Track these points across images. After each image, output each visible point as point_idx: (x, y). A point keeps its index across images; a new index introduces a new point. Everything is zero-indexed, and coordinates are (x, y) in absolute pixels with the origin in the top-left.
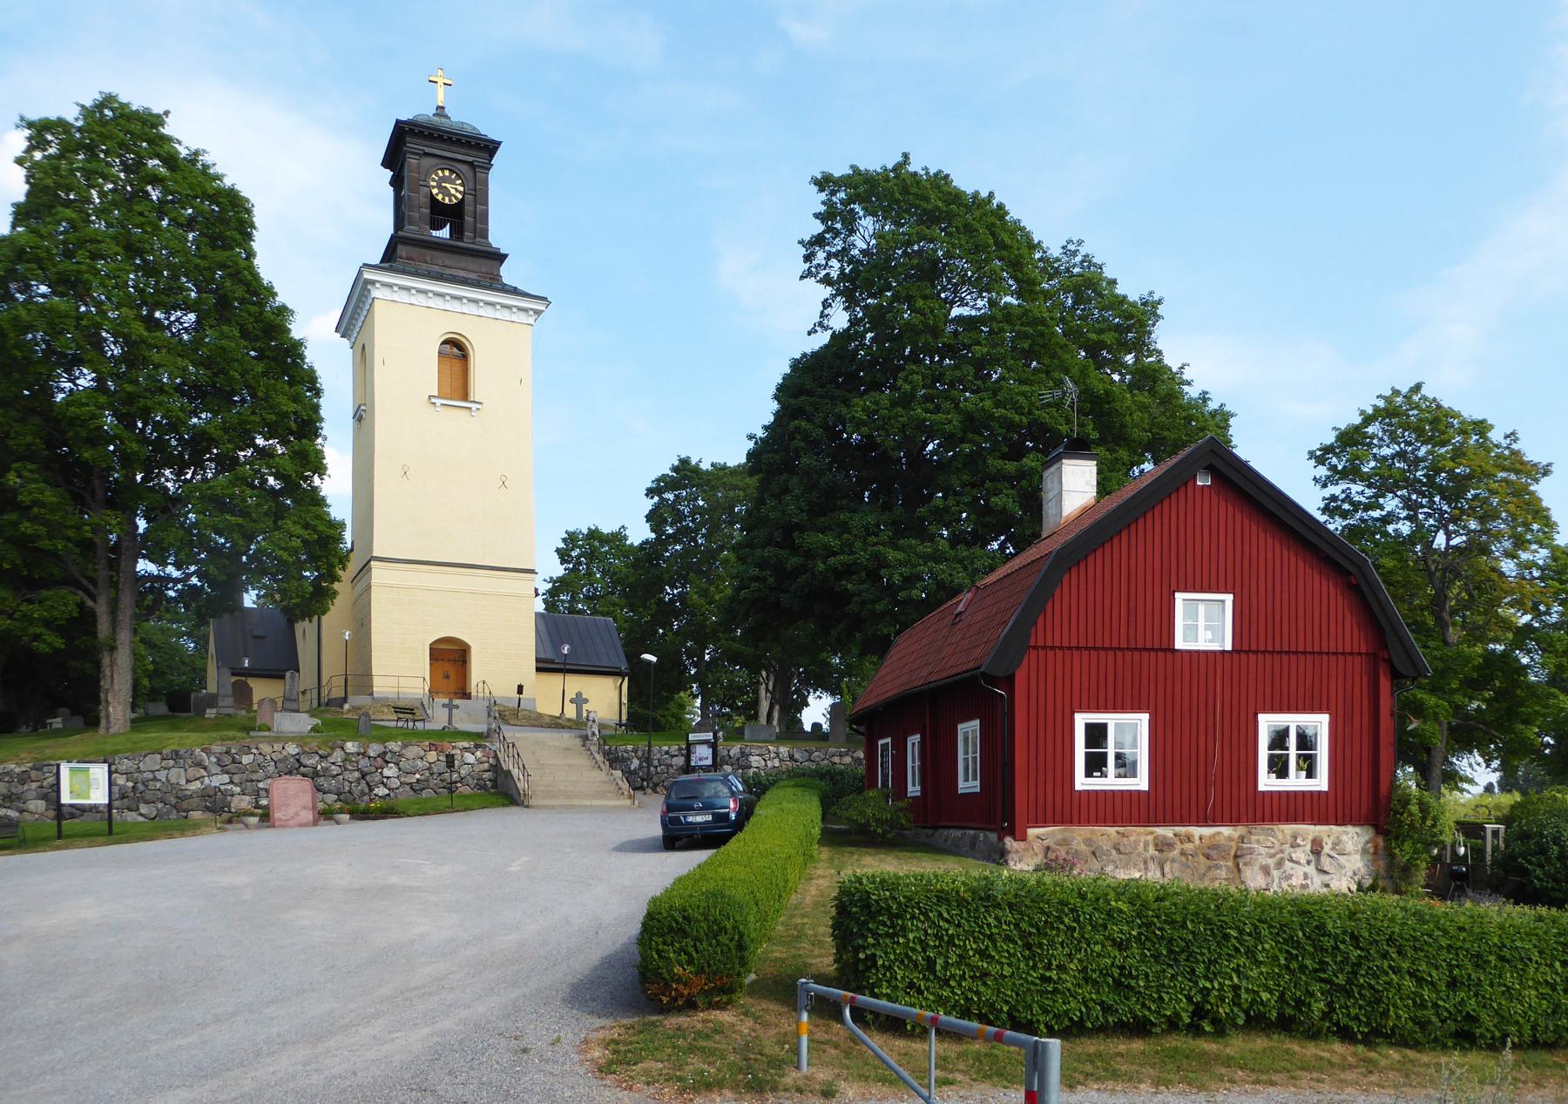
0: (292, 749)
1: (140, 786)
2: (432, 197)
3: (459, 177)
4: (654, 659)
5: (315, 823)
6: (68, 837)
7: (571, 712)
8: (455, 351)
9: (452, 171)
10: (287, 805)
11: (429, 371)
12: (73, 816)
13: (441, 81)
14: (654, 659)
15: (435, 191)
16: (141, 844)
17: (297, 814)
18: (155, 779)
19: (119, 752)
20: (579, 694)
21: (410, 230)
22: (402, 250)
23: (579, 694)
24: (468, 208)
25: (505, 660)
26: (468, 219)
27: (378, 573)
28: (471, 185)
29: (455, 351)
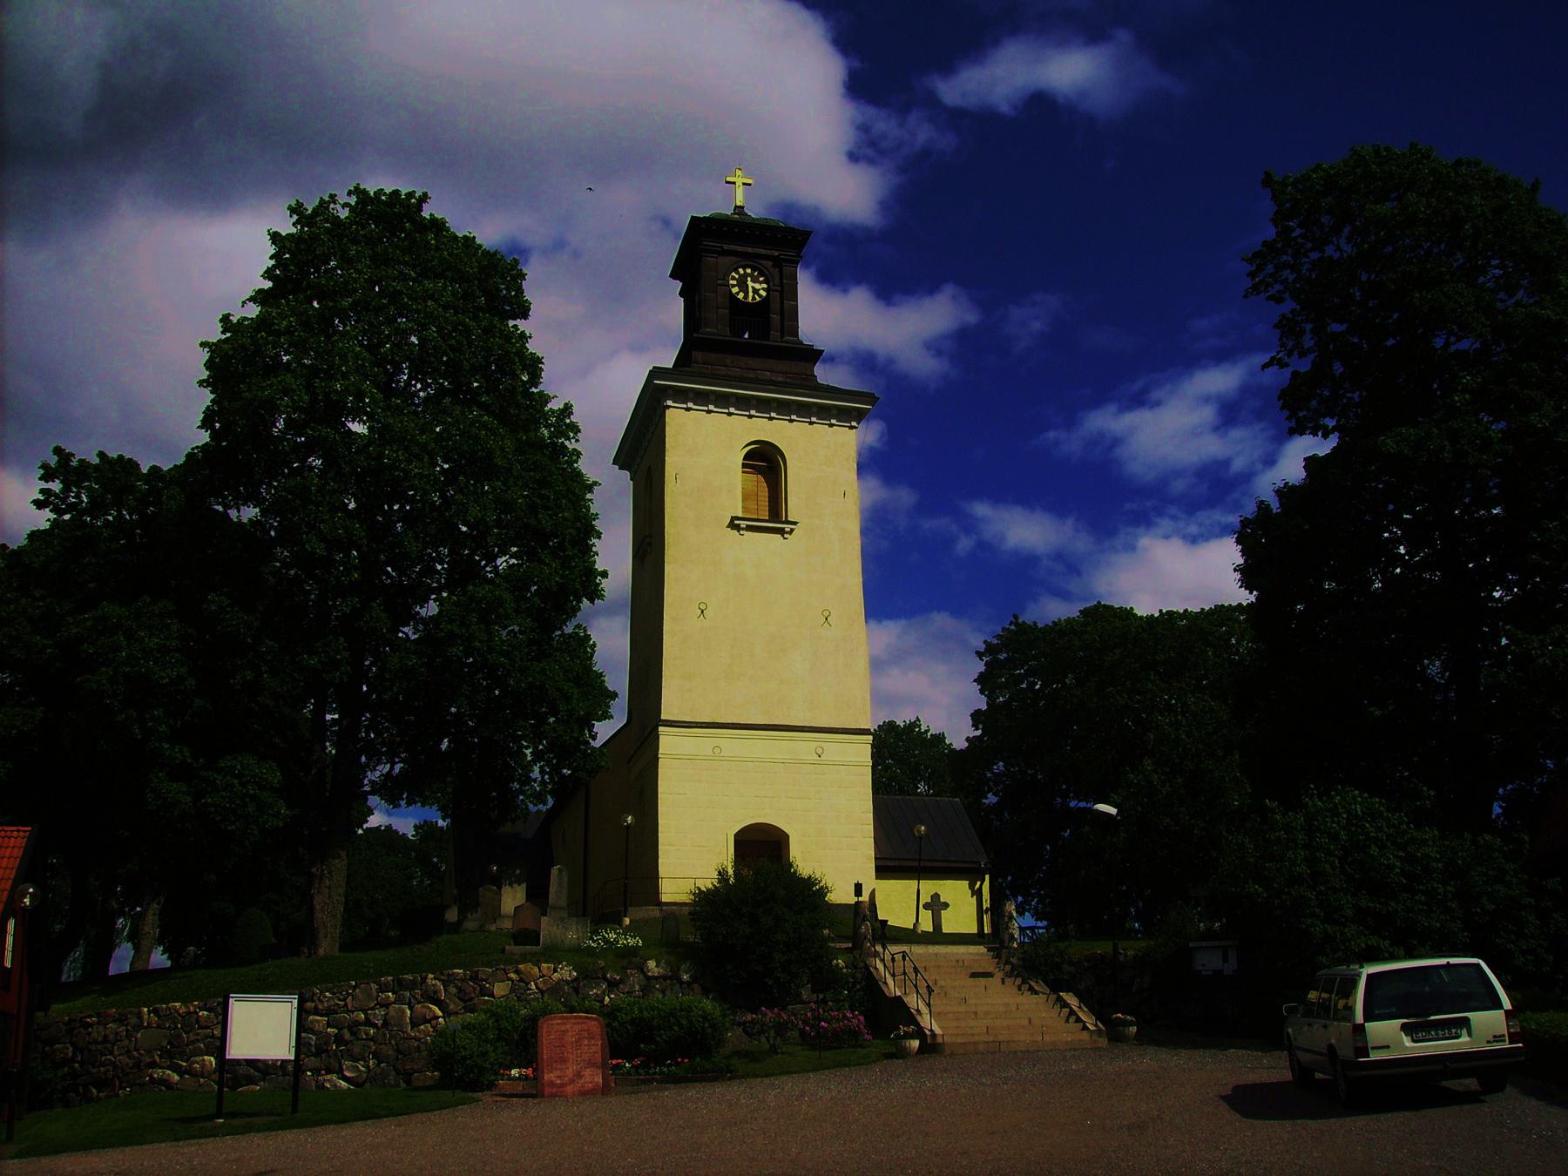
0: (566, 973)
1: (347, 1035)
2: (733, 297)
3: (761, 274)
4: (1113, 811)
5: (605, 1090)
6: (234, 1115)
7: (926, 925)
8: (765, 462)
9: (754, 270)
10: (564, 1061)
11: (732, 487)
12: (251, 1080)
13: (739, 181)
14: (1113, 811)
15: (735, 290)
16: (346, 1131)
17: (579, 1075)
18: (368, 1023)
19: (429, 1088)
20: (936, 896)
21: (708, 331)
22: (697, 355)
23: (936, 896)
24: (775, 306)
25: (836, 848)
26: (775, 318)
27: (669, 742)
28: (777, 282)
29: (765, 462)
